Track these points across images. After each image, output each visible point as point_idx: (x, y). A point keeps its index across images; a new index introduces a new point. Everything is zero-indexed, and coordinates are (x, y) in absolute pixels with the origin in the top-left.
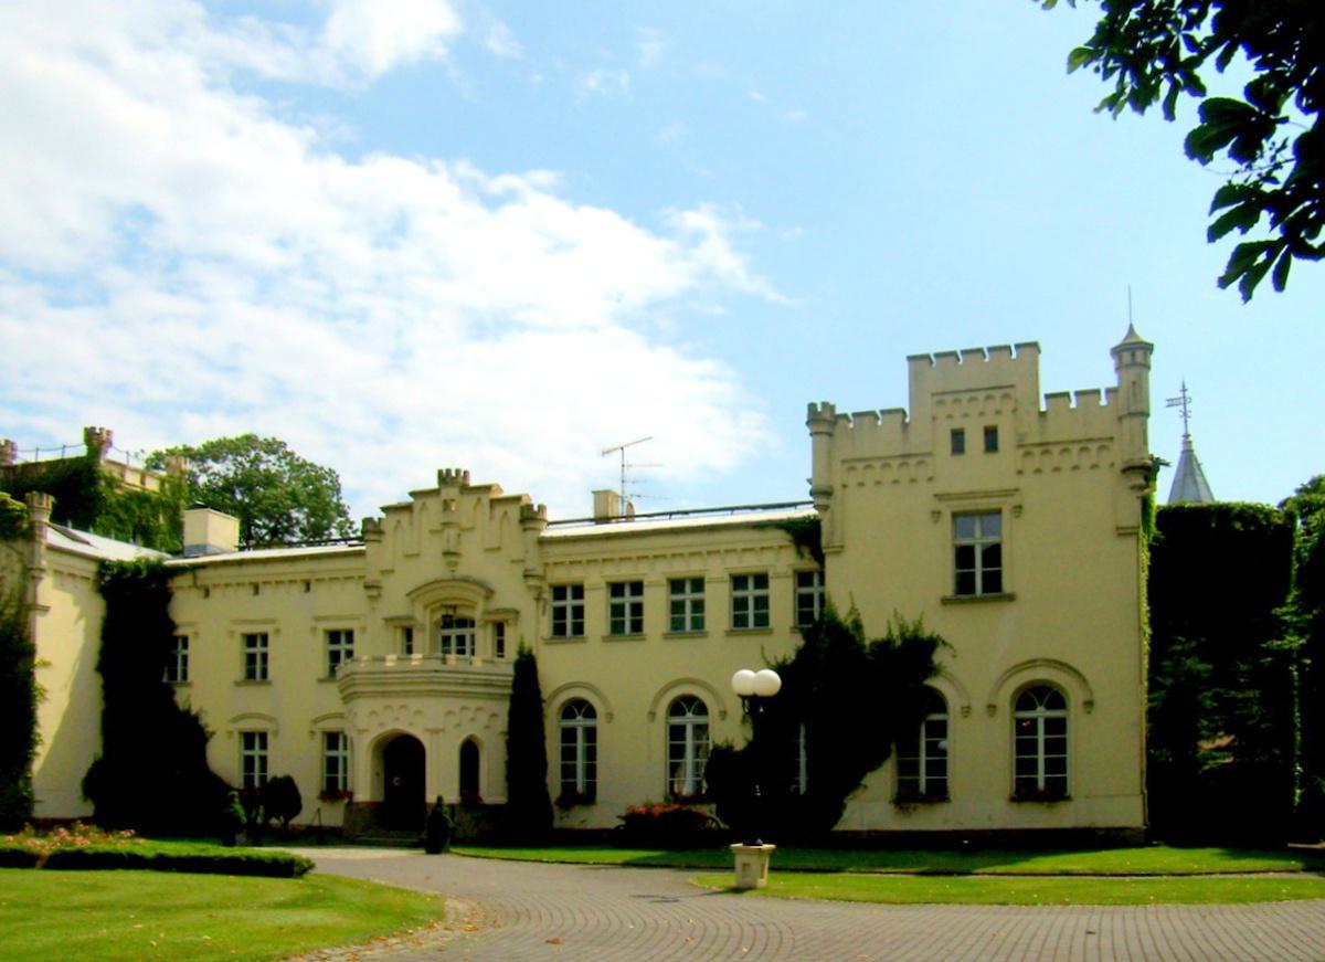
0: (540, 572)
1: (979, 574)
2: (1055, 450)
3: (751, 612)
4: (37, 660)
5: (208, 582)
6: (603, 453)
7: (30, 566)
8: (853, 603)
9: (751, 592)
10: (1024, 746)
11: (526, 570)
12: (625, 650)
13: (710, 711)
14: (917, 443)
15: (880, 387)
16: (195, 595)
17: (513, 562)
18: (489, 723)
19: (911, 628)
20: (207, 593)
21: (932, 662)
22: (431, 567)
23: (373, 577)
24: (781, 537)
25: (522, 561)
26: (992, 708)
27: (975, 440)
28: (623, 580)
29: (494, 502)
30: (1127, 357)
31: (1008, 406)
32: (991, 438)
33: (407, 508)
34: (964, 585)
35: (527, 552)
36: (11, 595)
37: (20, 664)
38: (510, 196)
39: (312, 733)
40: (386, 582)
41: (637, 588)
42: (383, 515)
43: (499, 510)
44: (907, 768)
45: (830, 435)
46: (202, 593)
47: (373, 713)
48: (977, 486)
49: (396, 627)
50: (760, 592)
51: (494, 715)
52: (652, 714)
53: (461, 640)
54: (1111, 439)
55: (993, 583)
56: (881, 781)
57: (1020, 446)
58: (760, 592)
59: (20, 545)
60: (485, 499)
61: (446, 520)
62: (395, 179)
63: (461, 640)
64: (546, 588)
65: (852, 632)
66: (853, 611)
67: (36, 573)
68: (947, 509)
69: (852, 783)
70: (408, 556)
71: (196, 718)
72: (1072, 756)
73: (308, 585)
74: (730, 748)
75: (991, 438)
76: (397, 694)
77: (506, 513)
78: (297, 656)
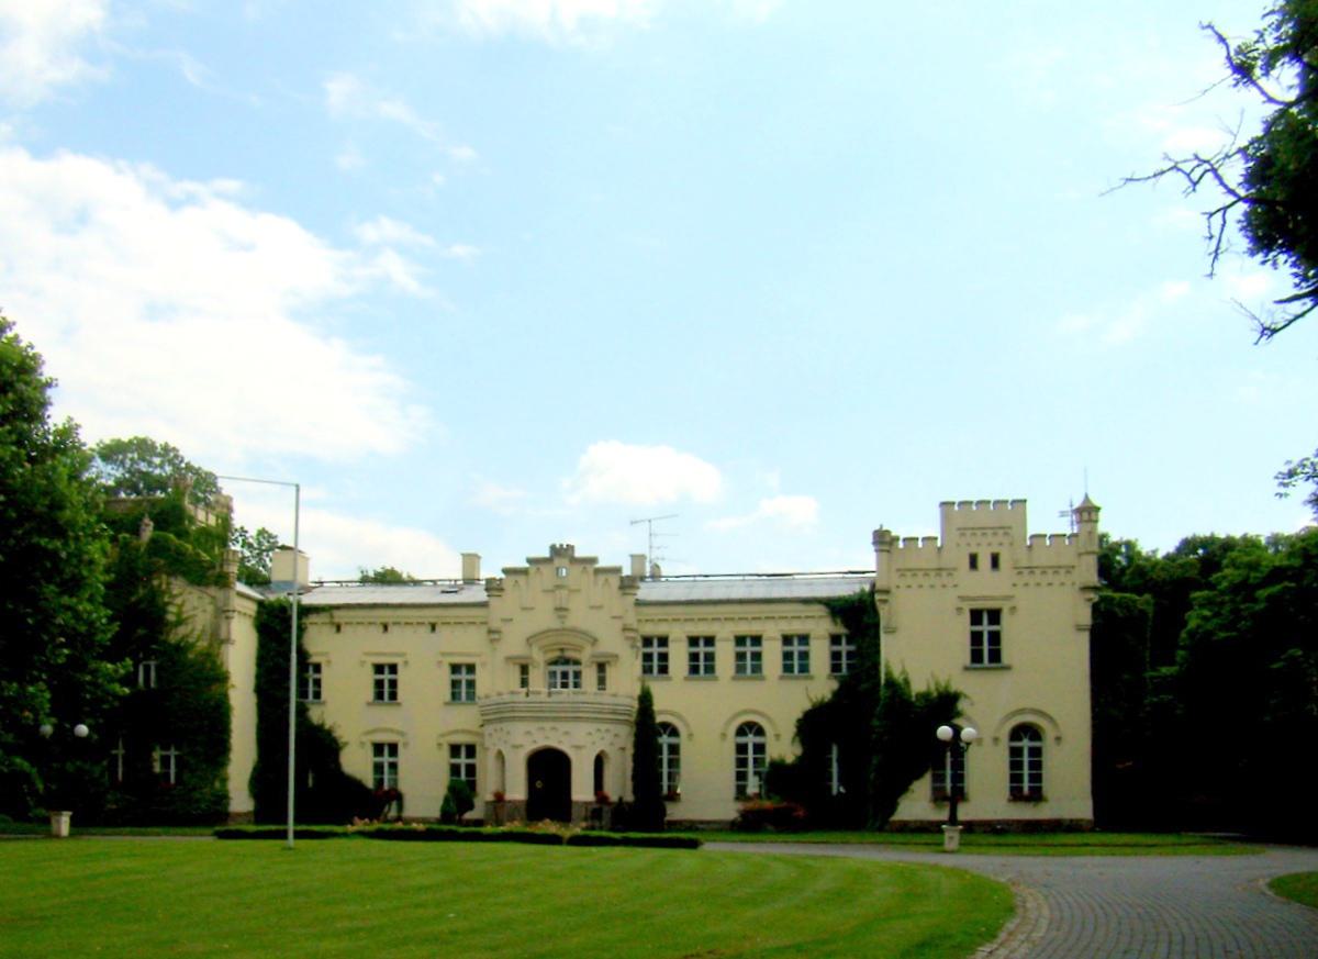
0: (635, 626)
1: (986, 648)
2: (1038, 571)
3: (796, 663)
4: (229, 685)
5: (342, 621)
6: (632, 523)
7: (226, 608)
8: (903, 667)
9: (796, 648)
10: (1015, 765)
11: (625, 625)
12: (701, 688)
13: (768, 734)
14: (948, 560)
15: (919, 523)
16: (328, 631)
17: (614, 617)
18: (618, 744)
19: (943, 684)
20: (338, 628)
21: (956, 708)
22: (544, 619)
23: (495, 624)
24: (820, 610)
25: (620, 617)
26: (996, 740)
27: (984, 562)
28: (698, 636)
29: (598, 571)
30: (1085, 516)
31: (1006, 541)
32: (995, 561)
33: (524, 572)
34: (976, 656)
35: (627, 611)
36: (203, 631)
37: (213, 688)
38: (191, 200)
39: (440, 745)
40: (505, 628)
41: (710, 641)
42: (503, 576)
43: (602, 578)
44: (938, 779)
45: (888, 551)
46: (334, 629)
47: (528, 733)
48: (986, 593)
49: (515, 664)
50: (803, 648)
51: (616, 735)
52: (724, 735)
53: (565, 675)
54: (1073, 567)
55: (995, 656)
56: (922, 788)
57: (1016, 568)
58: (803, 648)
59: (213, 590)
60: (590, 569)
61: (559, 583)
62: (80, 174)
63: (565, 675)
64: (639, 638)
65: (903, 686)
66: (903, 672)
67: (230, 614)
68: (967, 606)
69: (903, 788)
70: (524, 609)
71: (329, 733)
72: (1045, 772)
73: (386, 628)
74: (783, 761)
75: (995, 561)
76: (546, 719)
77: (607, 580)
78: (423, 683)
